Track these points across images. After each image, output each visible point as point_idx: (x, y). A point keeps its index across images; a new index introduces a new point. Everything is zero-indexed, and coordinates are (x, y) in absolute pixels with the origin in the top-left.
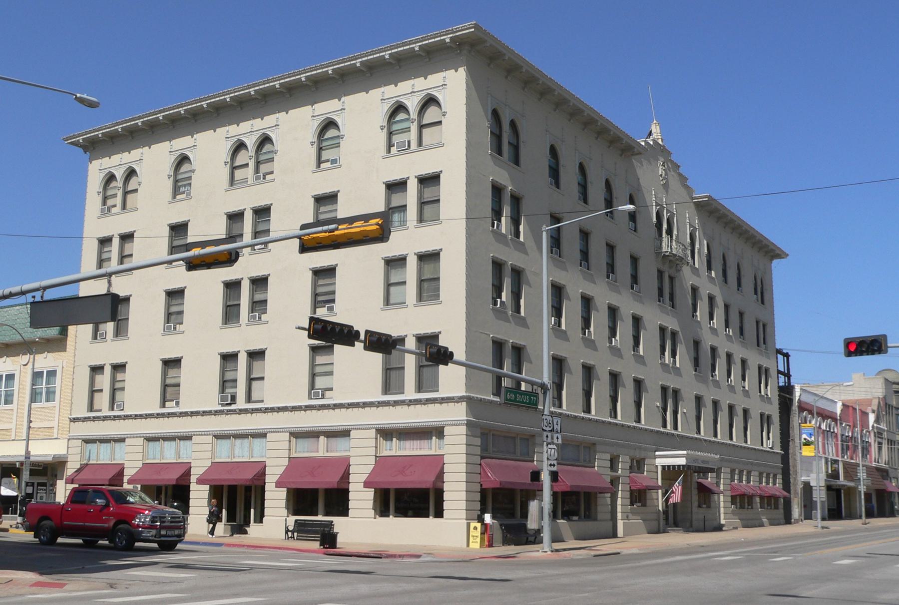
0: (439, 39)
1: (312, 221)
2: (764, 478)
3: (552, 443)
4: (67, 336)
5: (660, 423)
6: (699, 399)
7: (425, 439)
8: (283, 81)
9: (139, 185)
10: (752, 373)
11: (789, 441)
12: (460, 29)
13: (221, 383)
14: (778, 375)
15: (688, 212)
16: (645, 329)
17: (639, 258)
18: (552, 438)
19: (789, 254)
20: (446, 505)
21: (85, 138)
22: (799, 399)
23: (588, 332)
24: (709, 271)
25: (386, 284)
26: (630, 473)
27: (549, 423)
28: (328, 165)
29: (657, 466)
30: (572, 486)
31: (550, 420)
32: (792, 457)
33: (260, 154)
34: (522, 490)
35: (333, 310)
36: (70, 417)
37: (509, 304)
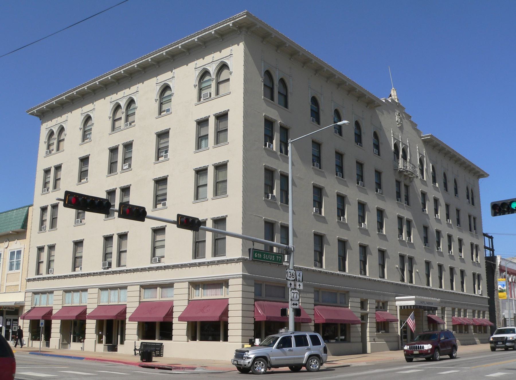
0: (226, 24)
2: (476, 314)
3: (295, 289)
4: (26, 229)
5: (399, 277)
6: (428, 264)
7: (218, 288)
8: (139, 63)
9: (65, 136)
10: (467, 248)
11: (494, 291)
12: (238, 16)
13: (104, 255)
14: (485, 250)
15: (392, 130)
16: (480, 251)
17: (289, 129)
18: (295, 285)
19: (490, 174)
20: (230, 333)
21: (37, 110)
22: (500, 265)
23: (343, 218)
24: (434, 183)
25: (196, 186)
26: (376, 311)
27: (293, 275)
28: (165, 113)
29: (397, 306)
30: (326, 320)
31: (293, 273)
32: (496, 300)
33: (128, 111)
34: (341, 324)
35: (166, 205)
36: (26, 278)
37: (278, 198)
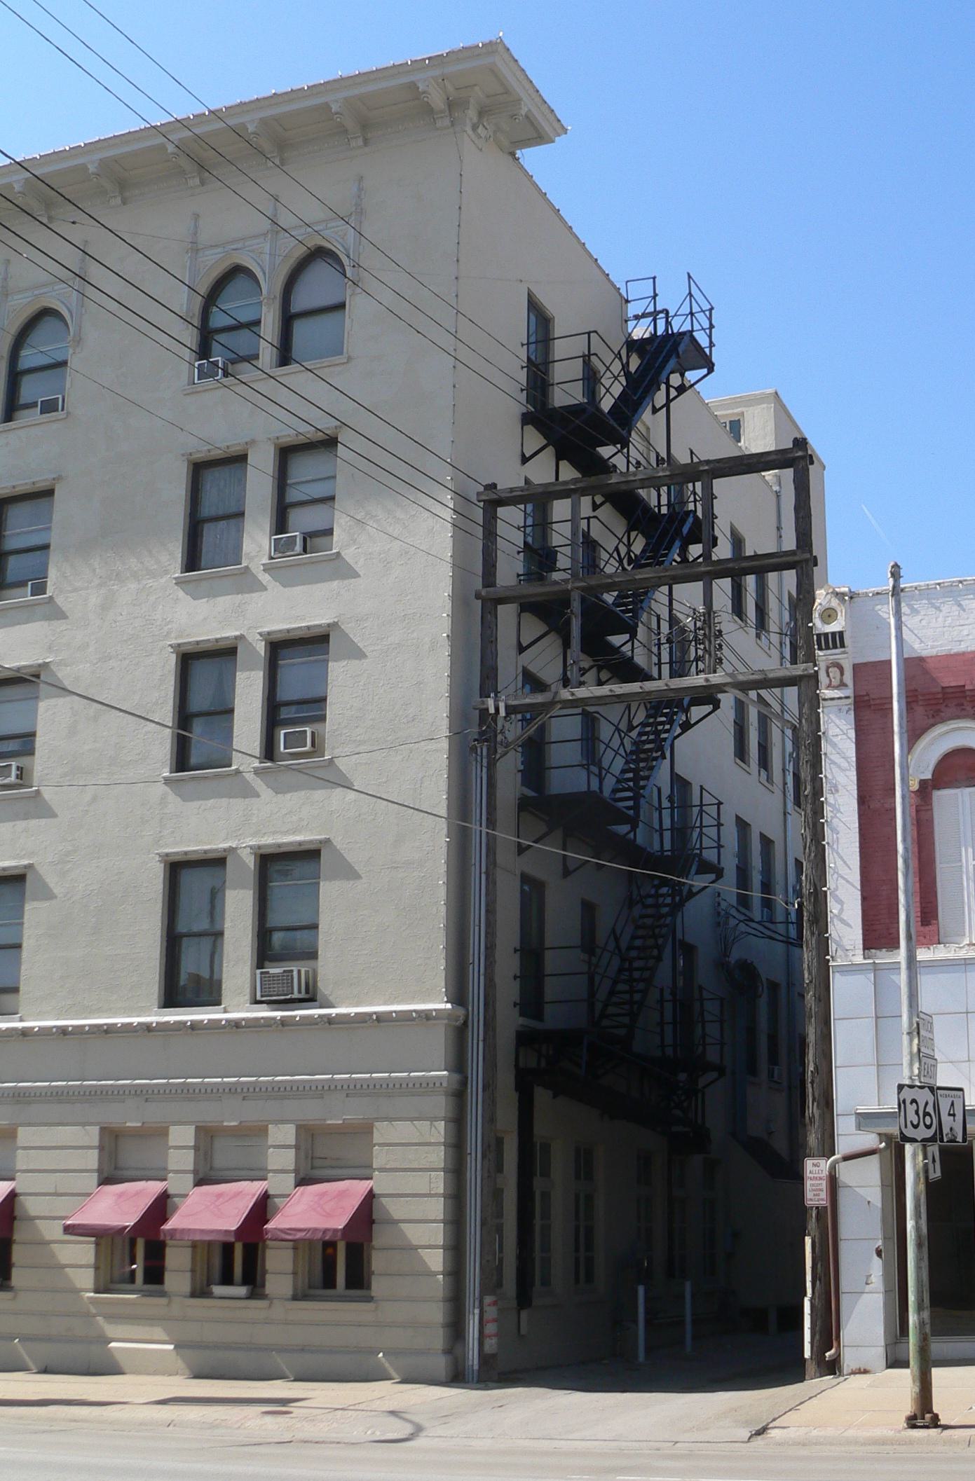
1: (555, 502)
27: (926, 1114)
31: (927, 1104)
